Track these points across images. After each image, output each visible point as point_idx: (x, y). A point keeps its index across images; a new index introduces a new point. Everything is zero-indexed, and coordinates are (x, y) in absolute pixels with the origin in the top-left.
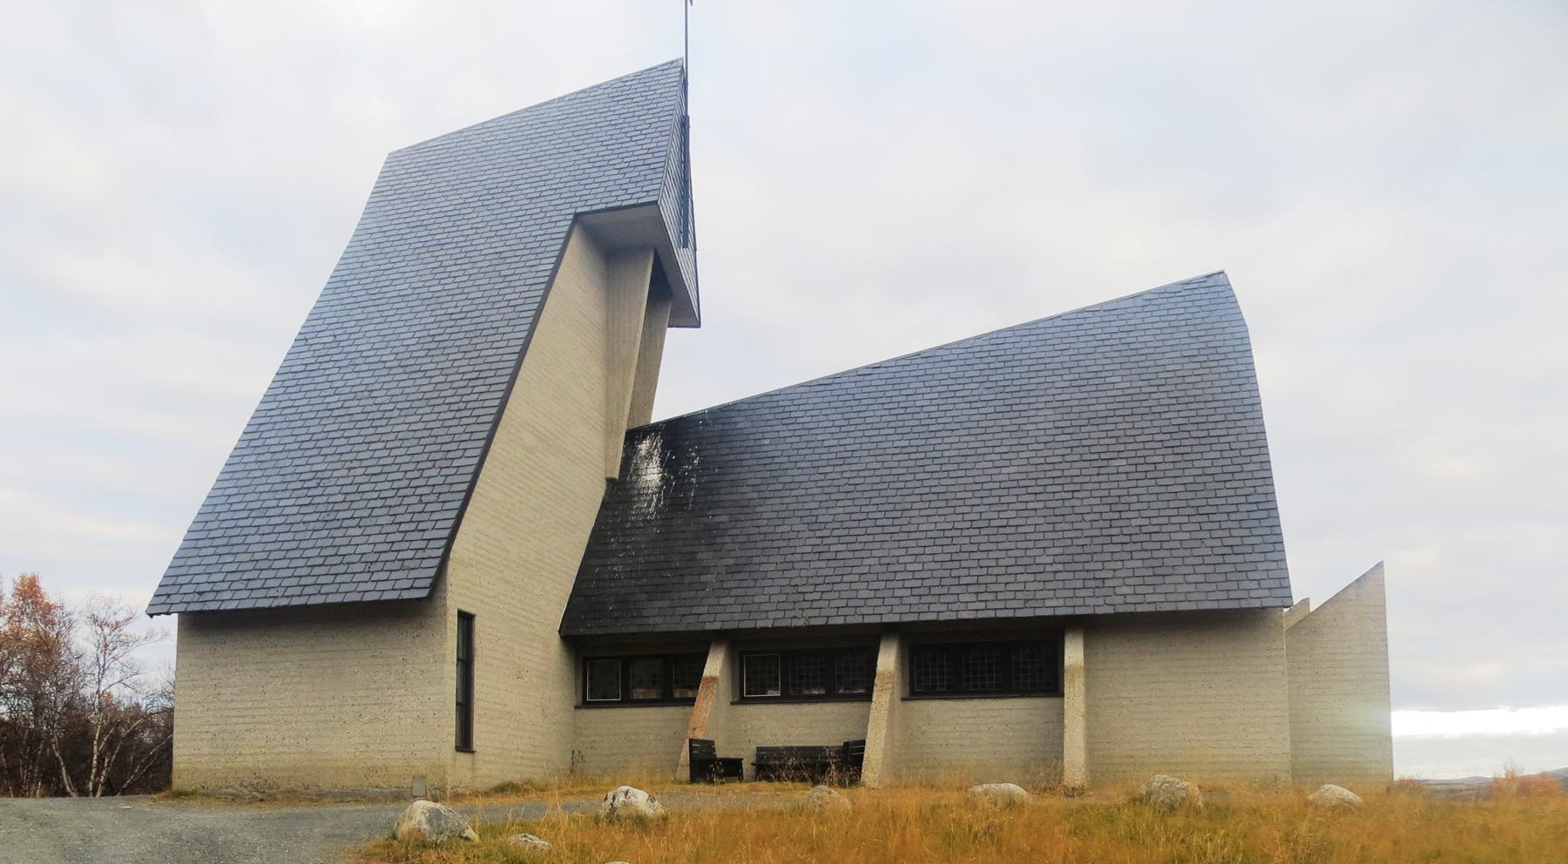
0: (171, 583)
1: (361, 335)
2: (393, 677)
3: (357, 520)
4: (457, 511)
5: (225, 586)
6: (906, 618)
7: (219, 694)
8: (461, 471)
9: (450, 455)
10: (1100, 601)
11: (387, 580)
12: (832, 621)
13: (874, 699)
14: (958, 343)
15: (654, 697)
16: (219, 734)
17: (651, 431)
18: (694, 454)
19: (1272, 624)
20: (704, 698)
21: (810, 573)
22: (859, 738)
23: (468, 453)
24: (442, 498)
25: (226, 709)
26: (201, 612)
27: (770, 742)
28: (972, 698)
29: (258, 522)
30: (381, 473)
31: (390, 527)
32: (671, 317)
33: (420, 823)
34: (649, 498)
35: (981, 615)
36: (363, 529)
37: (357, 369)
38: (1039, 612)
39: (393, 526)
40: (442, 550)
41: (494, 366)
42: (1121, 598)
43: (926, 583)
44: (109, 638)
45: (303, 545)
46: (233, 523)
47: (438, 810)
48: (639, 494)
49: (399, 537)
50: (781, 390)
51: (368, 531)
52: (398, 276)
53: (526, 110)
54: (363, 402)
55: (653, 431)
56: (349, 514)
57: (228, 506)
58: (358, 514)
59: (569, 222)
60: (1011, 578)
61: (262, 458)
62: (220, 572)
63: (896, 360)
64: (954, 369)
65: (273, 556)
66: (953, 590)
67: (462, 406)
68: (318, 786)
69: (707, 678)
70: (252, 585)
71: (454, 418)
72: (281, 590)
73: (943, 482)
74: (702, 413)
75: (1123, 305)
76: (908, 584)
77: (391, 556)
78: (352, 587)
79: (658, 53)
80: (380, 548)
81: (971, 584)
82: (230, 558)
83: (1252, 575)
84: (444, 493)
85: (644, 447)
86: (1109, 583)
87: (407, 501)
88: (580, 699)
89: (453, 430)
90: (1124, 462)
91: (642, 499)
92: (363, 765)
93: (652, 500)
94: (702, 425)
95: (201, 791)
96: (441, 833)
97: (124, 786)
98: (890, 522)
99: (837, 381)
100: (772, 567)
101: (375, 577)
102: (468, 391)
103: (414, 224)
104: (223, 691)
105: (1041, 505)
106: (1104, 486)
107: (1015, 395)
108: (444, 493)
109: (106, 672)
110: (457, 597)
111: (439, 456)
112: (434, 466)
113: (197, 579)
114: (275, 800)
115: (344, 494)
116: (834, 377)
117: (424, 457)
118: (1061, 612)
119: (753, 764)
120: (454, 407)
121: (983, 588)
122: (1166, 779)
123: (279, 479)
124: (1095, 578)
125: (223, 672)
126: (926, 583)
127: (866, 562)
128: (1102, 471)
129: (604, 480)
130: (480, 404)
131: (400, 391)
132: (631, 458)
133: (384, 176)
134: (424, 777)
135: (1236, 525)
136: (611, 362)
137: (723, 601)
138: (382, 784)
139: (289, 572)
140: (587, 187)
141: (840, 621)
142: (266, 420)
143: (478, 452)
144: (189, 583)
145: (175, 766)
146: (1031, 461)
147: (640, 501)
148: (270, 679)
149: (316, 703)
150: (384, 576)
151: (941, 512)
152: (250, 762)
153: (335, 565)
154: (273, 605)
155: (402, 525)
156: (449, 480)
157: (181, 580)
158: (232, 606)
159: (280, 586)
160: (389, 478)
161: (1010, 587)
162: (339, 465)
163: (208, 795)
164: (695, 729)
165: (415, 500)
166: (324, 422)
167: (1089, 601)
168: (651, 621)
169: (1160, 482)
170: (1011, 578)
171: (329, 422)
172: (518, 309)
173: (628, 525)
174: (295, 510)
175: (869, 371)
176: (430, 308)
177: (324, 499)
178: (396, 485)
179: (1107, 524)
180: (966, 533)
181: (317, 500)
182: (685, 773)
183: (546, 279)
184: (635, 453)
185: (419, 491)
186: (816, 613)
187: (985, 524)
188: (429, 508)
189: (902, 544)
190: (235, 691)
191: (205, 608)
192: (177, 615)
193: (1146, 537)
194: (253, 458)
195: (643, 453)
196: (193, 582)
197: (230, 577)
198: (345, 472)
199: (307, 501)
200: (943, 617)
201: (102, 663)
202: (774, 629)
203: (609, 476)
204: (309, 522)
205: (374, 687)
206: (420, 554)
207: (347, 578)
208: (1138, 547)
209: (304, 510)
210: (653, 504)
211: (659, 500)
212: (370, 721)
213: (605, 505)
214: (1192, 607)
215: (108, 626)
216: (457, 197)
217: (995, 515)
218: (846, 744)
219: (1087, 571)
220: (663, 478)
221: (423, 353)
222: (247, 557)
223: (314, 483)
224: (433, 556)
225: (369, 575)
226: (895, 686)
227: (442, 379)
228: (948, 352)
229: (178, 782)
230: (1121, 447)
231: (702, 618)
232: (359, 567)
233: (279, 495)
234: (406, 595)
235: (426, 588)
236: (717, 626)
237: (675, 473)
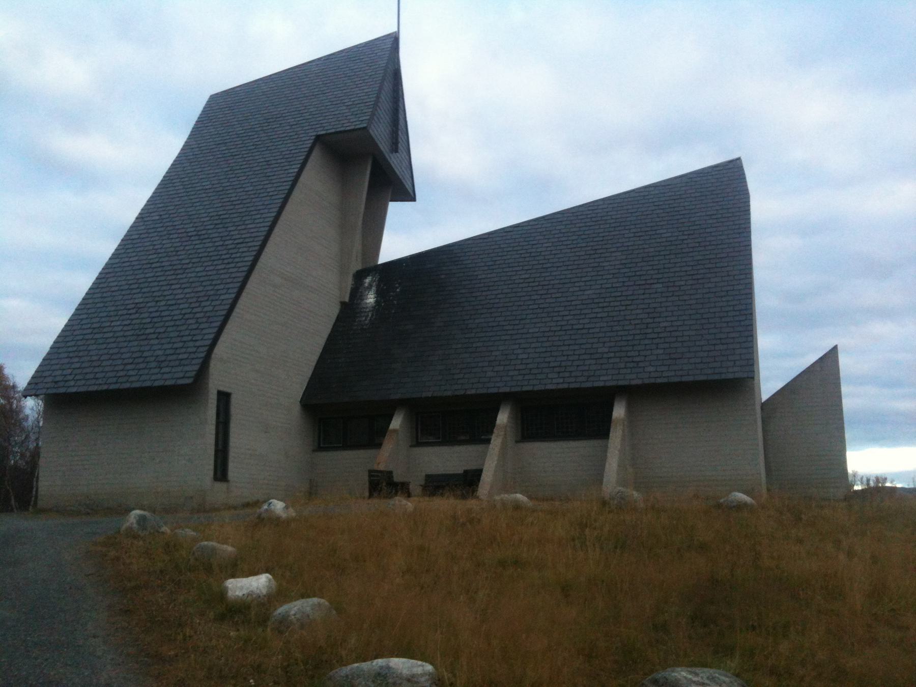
6: (513, 390)
10: (634, 376)
12: (469, 392)
18: (397, 285)
23: (230, 291)
33: (132, 524)
35: (561, 386)
42: (649, 373)
43: (529, 366)
47: (145, 516)
48: (361, 312)
52: (204, 176)
57: (80, 326)
60: (581, 363)
70: (88, 377)
73: (547, 301)
80: (168, 352)
83: (730, 358)
85: (368, 280)
90: (661, 285)
98: (511, 327)
110: (217, 381)
119: (421, 486)
120: (226, 261)
124: (633, 362)
126: (529, 366)
130: (241, 259)
134: (192, 498)
135: (725, 325)
141: (473, 392)
150: (167, 370)
157: (45, 374)
158: (74, 390)
159: (104, 377)
170: (581, 363)
183: (292, 178)
187: (570, 327)
188: (202, 326)
195: (366, 285)
203: (342, 300)
208: (662, 340)
209: (125, 328)
210: (369, 318)
211: (373, 315)
218: (466, 472)
219: (629, 357)
220: (376, 302)
230: (660, 276)
232: (153, 365)
236: (398, 396)
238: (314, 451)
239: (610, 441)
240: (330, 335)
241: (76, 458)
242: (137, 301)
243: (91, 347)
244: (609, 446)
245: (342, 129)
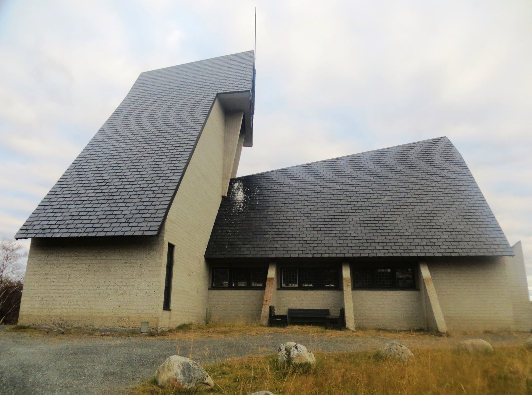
0: (30, 224)
2: (135, 273)
3: (123, 200)
4: (171, 198)
5: (56, 226)
7: (47, 278)
8: (172, 181)
9: (167, 175)
11: (137, 226)
14: (354, 155)
15: (243, 285)
16: (45, 298)
18: (256, 189)
20: (269, 287)
21: (311, 235)
24: (164, 192)
25: (50, 286)
26: (43, 238)
27: (294, 307)
28: (380, 290)
29: (75, 199)
30: (135, 181)
31: (139, 203)
33: (176, 374)
35: (387, 255)
36: (125, 204)
39: (140, 203)
40: (164, 214)
44: (9, 255)
45: (96, 210)
46: (63, 199)
48: (235, 203)
49: (143, 207)
50: (289, 168)
51: (128, 205)
55: (239, 180)
56: (119, 197)
58: (123, 197)
59: (215, 96)
62: (54, 220)
63: (332, 159)
65: (81, 214)
67: (172, 156)
68: (93, 326)
69: (269, 278)
70: (69, 226)
71: (169, 161)
74: (259, 174)
75: (412, 145)
77: (139, 216)
78: (119, 229)
80: (133, 212)
81: (379, 243)
82: (60, 214)
84: (164, 190)
85: (236, 185)
87: (147, 192)
88: (211, 286)
91: (237, 204)
92: (117, 315)
93: (241, 205)
94: (259, 179)
95: (32, 326)
96: (191, 381)
97: (8, 313)
99: (310, 165)
100: (295, 233)
104: (49, 277)
108: (164, 190)
109: (6, 268)
110: (168, 237)
111: (162, 175)
112: (160, 179)
113: (42, 223)
114: (70, 333)
115: (117, 189)
116: (309, 164)
117: (155, 175)
123: (87, 182)
125: (51, 268)
128: (421, 201)
131: (145, 150)
132: (231, 189)
133: (139, 79)
137: (275, 246)
138: (125, 326)
140: (174, 138)
141: (327, 255)
142: (84, 159)
143: (180, 174)
144: (39, 225)
145: (20, 313)
147: (236, 205)
148: (74, 272)
149: (96, 284)
150: (135, 224)
152: (58, 312)
153: (111, 219)
154: (79, 236)
155: (145, 203)
156: (167, 185)
157: (34, 223)
158: (58, 235)
159: (83, 227)
160: (139, 183)
162: (115, 177)
163: (35, 329)
167: (431, 251)
168: (245, 253)
173: (232, 214)
174: (94, 195)
175: (322, 163)
176: (158, 121)
177: (107, 191)
178: (142, 186)
181: (104, 191)
182: (265, 321)
184: (232, 187)
185: (153, 189)
188: (158, 196)
190: (55, 277)
191: (45, 236)
192: (31, 239)
194: (76, 173)
195: (236, 187)
196: (40, 224)
197: (59, 223)
198: (118, 180)
199: (100, 191)
201: (5, 264)
202: (299, 258)
203: (223, 195)
204: (100, 200)
205: (125, 277)
206: (153, 215)
207: (117, 225)
210: (242, 207)
211: (244, 205)
212: (122, 294)
214: (474, 254)
215: (9, 250)
220: (245, 197)
222: (68, 214)
223: (103, 184)
224: (159, 216)
225: (128, 224)
229: (22, 320)
231: (267, 253)
234: (146, 233)
235: (156, 230)
237: (250, 195)
238: (209, 289)
239: (345, 292)
240: (217, 215)
241: (53, 288)
242: (104, 178)
243: (70, 206)
244: (429, 296)
245: (233, 91)
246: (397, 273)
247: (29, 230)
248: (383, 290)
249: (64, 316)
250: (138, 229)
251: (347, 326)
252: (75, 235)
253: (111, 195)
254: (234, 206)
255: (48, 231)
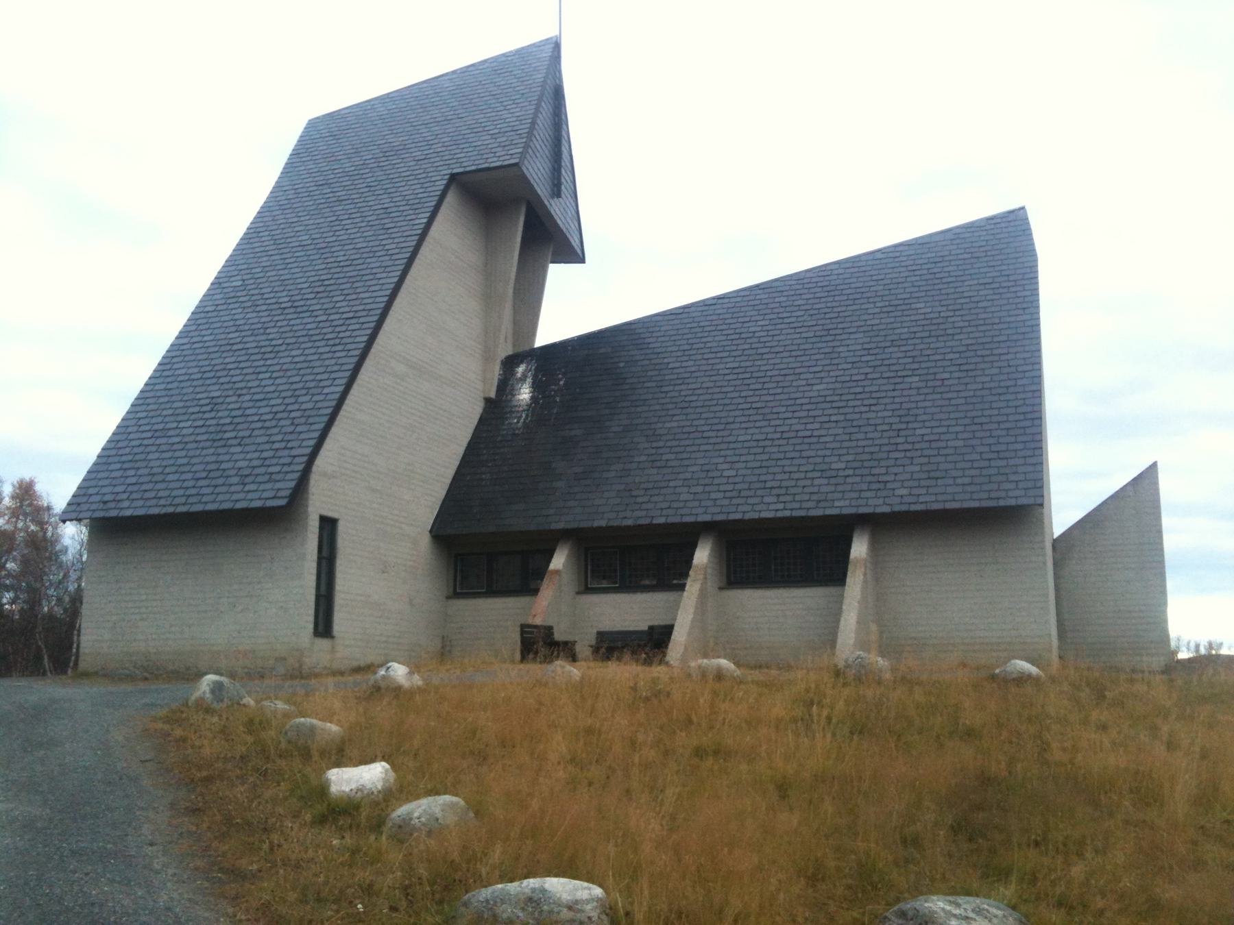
1: (264, 280)
5: (125, 496)
9: (322, 384)
10: (881, 501)
13: (686, 589)
17: (527, 356)
19: (1035, 520)
22: (668, 623)
23: (336, 382)
25: (125, 601)
26: (104, 519)
28: (778, 587)
30: (264, 399)
32: (553, 254)
33: (204, 693)
34: (519, 415)
35: (779, 514)
37: (258, 309)
38: (828, 512)
41: (368, 307)
48: (511, 412)
53: (424, 82)
54: (258, 338)
55: (530, 356)
59: (445, 182)
61: (170, 386)
64: (785, 299)
66: (759, 493)
68: (197, 668)
72: (170, 500)
76: (722, 488)
79: (550, 32)
85: (521, 369)
86: (889, 486)
88: (451, 590)
89: (327, 362)
91: (514, 415)
93: (521, 416)
101: (247, 488)
102: (344, 328)
103: (321, 183)
105: (842, 418)
106: (897, 400)
107: (833, 321)
110: (319, 502)
118: (846, 511)
119: (591, 646)
120: (331, 342)
121: (783, 491)
122: (859, 655)
127: (690, 469)
128: (898, 387)
129: (483, 400)
132: (509, 380)
133: (302, 141)
134: (285, 659)
136: (489, 298)
139: (178, 485)
146: (839, 379)
151: (758, 424)
158: (128, 513)
161: (806, 490)
164: (535, 616)
165: (288, 422)
166: (225, 355)
169: (945, 396)
171: (229, 355)
172: (394, 257)
176: (324, 256)
179: (895, 434)
180: (776, 442)
183: (419, 232)
186: (644, 513)
187: (793, 434)
188: (299, 429)
189: (722, 453)
191: (107, 515)
193: (927, 445)
194: (162, 386)
195: (519, 375)
197: (130, 489)
200: (747, 517)
203: (487, 396)
204: (200, 441)
206: (286, 469)
209: (198, 431)
210: (522, 420)
211: (527, 416)
213: (481, 421)
216: (359, 159)
217: (802, 427)
218: (651, 628)
220: (532, 398)
221: (312, 296)
222: (146, 471)
226: (868, 571)
227: (324, 318)
228: (782, 283)
229: (83, 665)
232: (235, 480)
233: (180, 418)
234: (270, 503)
238: (448, 598)
241: (130, 605)
243: (151, 456)
245: (486, 165)
246: (18, 570)
247: (82, 505)
248: (784, 587)
249: (149, 653)
250: (256, 495)
251: (668, 658)
252: (155, 511)
253: (220, 431)
254: (507, 419)
255: (112, 505)
